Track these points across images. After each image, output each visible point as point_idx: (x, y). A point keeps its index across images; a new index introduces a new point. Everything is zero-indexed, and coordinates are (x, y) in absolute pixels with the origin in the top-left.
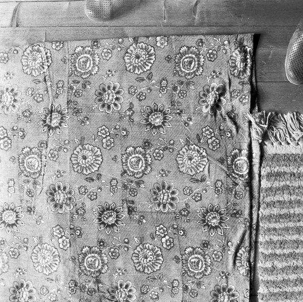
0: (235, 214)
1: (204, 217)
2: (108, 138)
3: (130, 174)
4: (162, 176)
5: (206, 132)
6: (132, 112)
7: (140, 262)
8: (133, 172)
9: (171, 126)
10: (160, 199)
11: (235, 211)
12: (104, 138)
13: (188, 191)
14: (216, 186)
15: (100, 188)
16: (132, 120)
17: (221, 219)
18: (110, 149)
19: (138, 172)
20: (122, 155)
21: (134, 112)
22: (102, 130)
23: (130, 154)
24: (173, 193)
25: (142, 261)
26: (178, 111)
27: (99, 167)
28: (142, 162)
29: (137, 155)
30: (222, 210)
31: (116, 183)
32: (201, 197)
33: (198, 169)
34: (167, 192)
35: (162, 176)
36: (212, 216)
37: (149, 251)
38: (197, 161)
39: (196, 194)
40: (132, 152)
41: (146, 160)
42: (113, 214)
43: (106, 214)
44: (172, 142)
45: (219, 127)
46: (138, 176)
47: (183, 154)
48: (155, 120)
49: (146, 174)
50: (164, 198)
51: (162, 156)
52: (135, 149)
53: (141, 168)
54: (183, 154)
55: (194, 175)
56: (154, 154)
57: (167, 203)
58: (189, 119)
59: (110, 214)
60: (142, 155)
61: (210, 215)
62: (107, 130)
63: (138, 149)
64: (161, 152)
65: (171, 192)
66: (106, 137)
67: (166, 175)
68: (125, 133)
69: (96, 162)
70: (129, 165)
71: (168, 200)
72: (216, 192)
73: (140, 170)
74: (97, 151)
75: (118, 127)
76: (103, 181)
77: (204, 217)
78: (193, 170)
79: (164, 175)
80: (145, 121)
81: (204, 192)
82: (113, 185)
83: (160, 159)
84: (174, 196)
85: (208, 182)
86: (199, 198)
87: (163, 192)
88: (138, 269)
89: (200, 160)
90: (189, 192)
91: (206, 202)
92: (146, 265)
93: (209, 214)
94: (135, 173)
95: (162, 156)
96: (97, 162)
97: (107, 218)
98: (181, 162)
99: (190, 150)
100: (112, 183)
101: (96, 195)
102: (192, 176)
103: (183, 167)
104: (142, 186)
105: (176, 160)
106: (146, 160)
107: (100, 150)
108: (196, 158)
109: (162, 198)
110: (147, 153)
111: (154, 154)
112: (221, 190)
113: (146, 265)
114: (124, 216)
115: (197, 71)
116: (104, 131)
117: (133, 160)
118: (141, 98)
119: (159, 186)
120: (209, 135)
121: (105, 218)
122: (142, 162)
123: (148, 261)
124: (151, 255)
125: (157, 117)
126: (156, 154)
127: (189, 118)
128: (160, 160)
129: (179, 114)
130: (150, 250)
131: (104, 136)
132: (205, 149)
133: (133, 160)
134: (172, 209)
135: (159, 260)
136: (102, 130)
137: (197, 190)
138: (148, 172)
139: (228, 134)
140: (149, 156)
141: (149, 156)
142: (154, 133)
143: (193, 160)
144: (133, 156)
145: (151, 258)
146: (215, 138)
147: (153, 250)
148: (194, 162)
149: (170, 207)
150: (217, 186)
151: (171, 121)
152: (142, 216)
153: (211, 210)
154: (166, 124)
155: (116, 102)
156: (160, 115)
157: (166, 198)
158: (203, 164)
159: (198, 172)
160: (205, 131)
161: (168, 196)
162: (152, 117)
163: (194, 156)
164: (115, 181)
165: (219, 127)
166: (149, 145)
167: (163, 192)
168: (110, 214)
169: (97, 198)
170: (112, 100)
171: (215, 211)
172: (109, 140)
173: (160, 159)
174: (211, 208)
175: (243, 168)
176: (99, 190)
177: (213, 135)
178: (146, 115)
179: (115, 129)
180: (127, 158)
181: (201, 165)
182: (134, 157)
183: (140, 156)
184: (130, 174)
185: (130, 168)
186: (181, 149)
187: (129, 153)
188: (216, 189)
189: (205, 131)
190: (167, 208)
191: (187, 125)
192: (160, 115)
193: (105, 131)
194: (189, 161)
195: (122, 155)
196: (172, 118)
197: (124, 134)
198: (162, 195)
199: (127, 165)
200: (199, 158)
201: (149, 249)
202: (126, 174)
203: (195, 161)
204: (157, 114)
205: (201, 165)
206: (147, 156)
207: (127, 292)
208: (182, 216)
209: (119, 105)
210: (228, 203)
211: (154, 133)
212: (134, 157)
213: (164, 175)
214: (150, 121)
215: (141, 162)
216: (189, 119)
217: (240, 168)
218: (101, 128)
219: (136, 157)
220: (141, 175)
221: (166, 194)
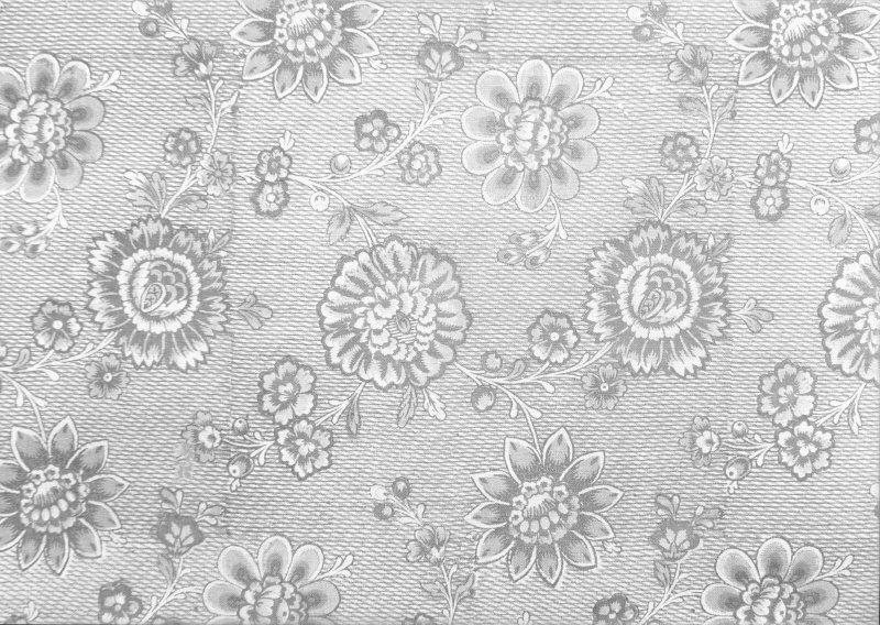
0: (201, 57)
1: (347, 39)
2: (784, 419)
3: (692, 243)
4: (536, 235)
5: (312, 447)
6: (663, 543)
7: (430, 300)
8: (677, 254)
9: (476, 477)
10: (551, 125)
11: (203, 69)
12: (804, 418)
13: (416, 165)
14: (285, 186)
15: (838, 174)
16: (664, 502)
17: (268, 30)
18: (780, 366)
19: (654, 252)
20: (724, 337)
21: (654, 540)
22: (813, 457)
23: (688, 339)
24: (488, 156)
25: (422, 303)
26: (436, 554)
27: (840, 275)
28: (629, 300)
29: (655, 334)
30: (265, 71)
31: (760, 202)
32: (360, 135)
33: (366, 269)
34: (518, 157)
35: (536, 235)
36: (311, 44)
37: (386, 351)
38: (372, 306)
39: (380, 146)
40: (679, 347)
41: (613, 311)
42: (785, 52)
43: (816, 50)
44: (485, 401)
45: (247, 471)
46: (653, 233)
47: (438, 346)
48: (552, 506)
49: (615, 243)
50: (535, 131)
51: (537, 332)
52: (664, 366)
53: (637, 275)
54: (438, 346)
55: (388, 241)
56: (572, 339)
57: (521, 106)
58: (387, 511)
59: (796, 51)
60: (630, 334)
61: (320, 45)
62: (786, 458)
63: (652, 361)
64: (539, 352)
65: (500, 161)
66: (796, 421)
67: (519, 239)
68: (700, 442)
69: (852, 302)
70: (694, 286)
71: (518, 120)
72: (285, 162)
73: (641, 261)
74: (842, 353)
75: (734, 470)
76: (821, 208)
77: (347, 39)
78: (391, 267)
79: (528, 239)
80: (600, 498)
81: (342, 160)
82: (777, 193)
83: (547, 320)
84: (487, 141)
85: (321, 205)
86: (367, 128)
87: (539, 155)
88: (445, 267)
89: (358, 311)
90: (412, 158)
91: (338, 104)
92: (403, 281)
93: (326, 53)
94: (665, 250)
95: (537, 332)
96: (845, 302)
97: (813, 30)
98: (444, 306)
99: (403, 363)
100: (779, 202)
101: (860, 140)
102: (393, 237)
103: (438, 282)
104: (635, 186)
105: (470, 317)
106: (613, 311)
107: (828, 358)
108: (376, 325)
109: (545, 131)
110: (607, 347)
111: (572, 339)
112: (264, 170)
113: (403, 281)
114: (730, 40)
115: (616, 267)
116: (804, 452)
117: (675, 312)
118: (616, 607)
119: (555, 186)
120: (302, 435)
121: (822, 30)
122: (629, 300)
123: (395, 303)
124: (378, 332)
125: (538, 518)
126: (563, 340)
127: (385, 518)
128: (547, 311)
129: (435, 542)
130: (379, 356)
131: (803, 427)
132: (334, 367)
133: (675, 312)
134: (496, 75)
135: (339, 309)
136: (813, 457)
137: (372, 169)
138: (601, 254)
139: (212, 438)
140: (597, 330)
141: (597, 330)
142: (560, 438)
143: (389, 313)
144: (672, 332)
145: (378, 317)
146: (278, 417)
147: (365, 357)
148: (386, 304)
149: (510, 87)
150: (279, 189)
151: (472, 504)
152: (646, 39)
153: (312, 69)
154: (502, 487)
155: (735, 588)
156: (524, 528)
157: (526, 132)
158: (344, 292)
159: (364, 257)
160: (315, 454)
161: (513, 140)
162: (564, 517)
163: (386, 334)
164: (764, 211)
165: (247, 471)
166: (597, 383)
167: (539, 155)
168: (796, 51)
169: (857, 129)
170: (755, 597)
171: (293, 68)
172: (782, 408)
173: (547, 320)
174: (312, 80)
175: (152, 278)
176: (842, 164)
177: (283, 435)
178: (592, 528)
179: (745, 463)
180: (700, 323)
181: (352, 287)
182: (670, 323)
183: (640, 332)
184: (692, 243)
185: (690, 274)
186: (444, 366)
187: (690, 342)
188: (283, 174)
189: (315, 454)
190: (522, 82)
191: (401, 486)
192: (524, 528)
193: (795, 451)
194: (407, 310)
195: (724, 337)
196: (468, 519)
197: (707, 434)
198: (542, 142)
199: (705, 288)
200: (359, 324)
201: (385, 361)
202: (711, 242)
203: (379, 309)
204: (543, 533)
205: (352, 287)
206: (605, 332)
207: (507, 149)
208: (448, 46)
209: (721, 572)
210: (235, 109)
211: (560, 438)
212: (670, 323)
213: (528, 239)
214: (575, 501)
215: (636, 302)
216: (387, 511)
217: (166, 281)
218: (818, 465)
219: (657, 326)
220: (637, 241)
221: (524, 146)
